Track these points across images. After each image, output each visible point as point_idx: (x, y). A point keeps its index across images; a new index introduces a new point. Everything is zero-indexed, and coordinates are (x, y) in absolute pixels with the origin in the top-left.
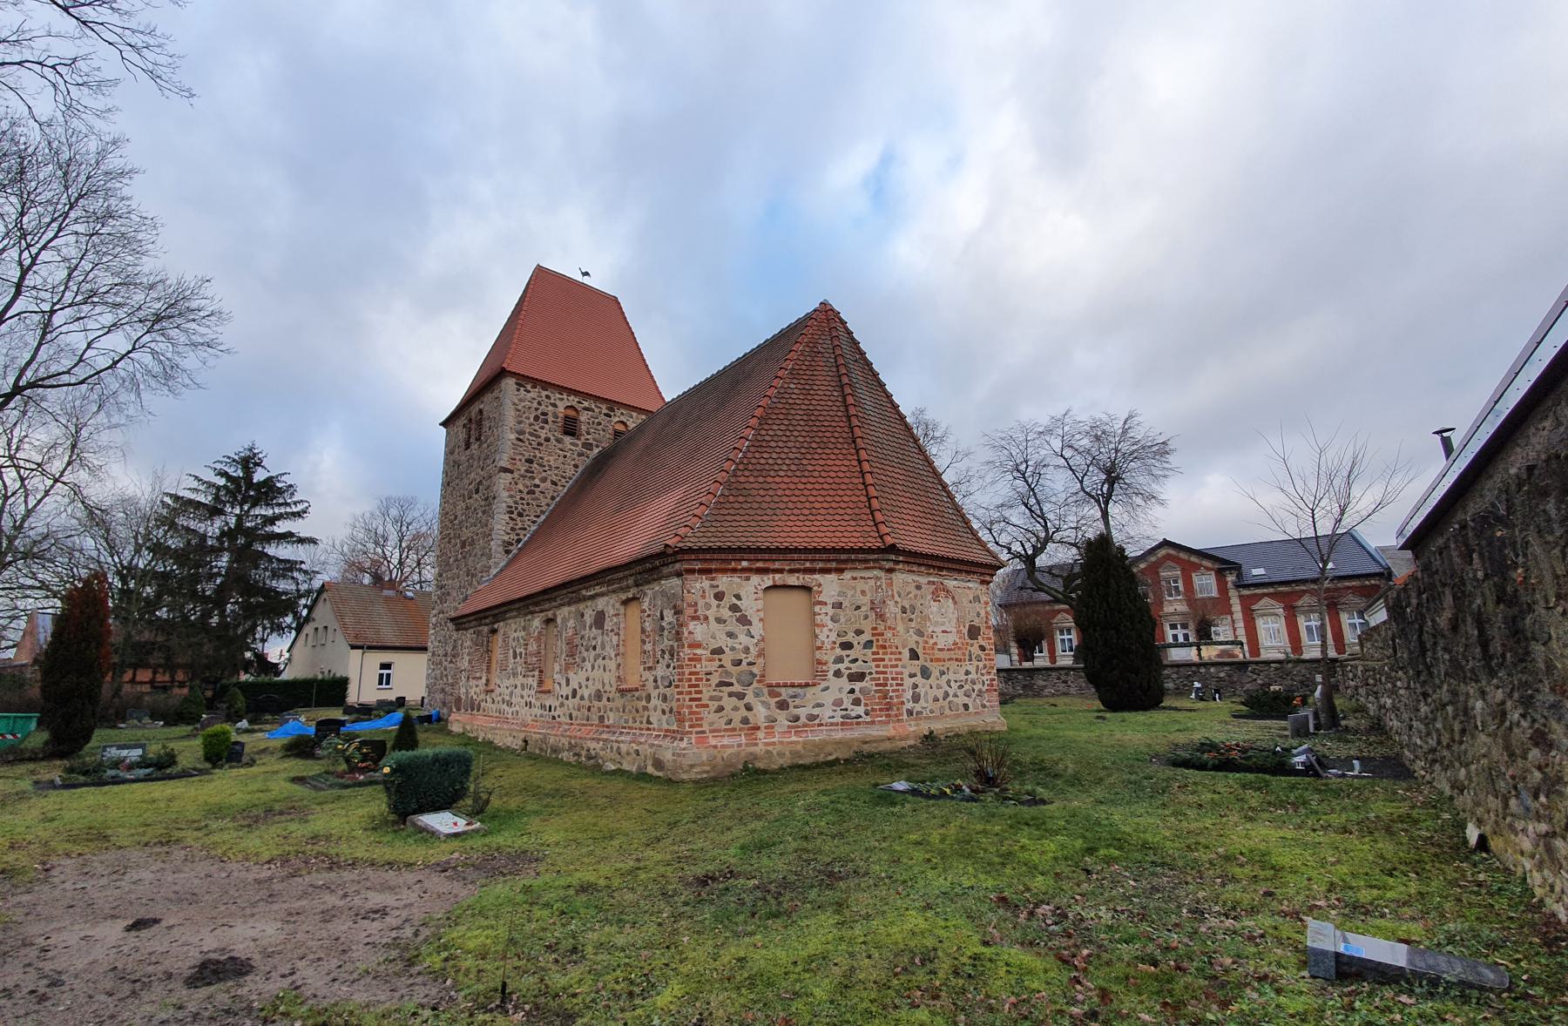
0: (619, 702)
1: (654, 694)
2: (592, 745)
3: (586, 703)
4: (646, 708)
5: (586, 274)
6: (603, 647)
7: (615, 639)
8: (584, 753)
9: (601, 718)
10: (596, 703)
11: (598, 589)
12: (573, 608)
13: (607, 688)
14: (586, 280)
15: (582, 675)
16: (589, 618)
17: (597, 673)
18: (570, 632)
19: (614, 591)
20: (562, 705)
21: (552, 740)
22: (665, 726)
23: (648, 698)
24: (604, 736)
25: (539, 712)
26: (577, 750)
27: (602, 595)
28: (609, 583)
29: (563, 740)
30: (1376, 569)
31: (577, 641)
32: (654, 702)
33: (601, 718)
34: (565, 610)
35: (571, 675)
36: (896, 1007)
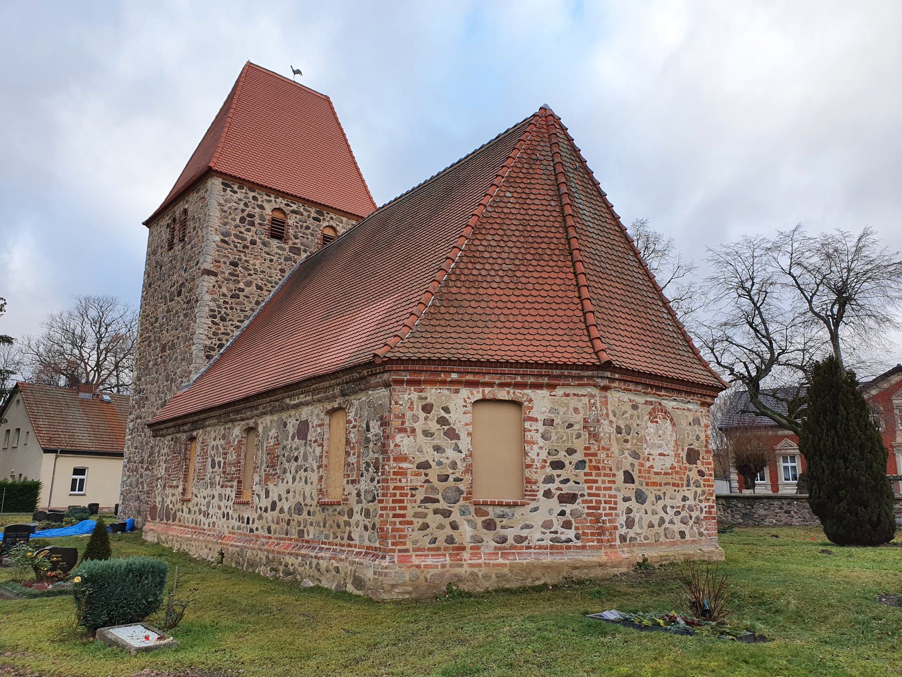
0: (319, 517)
1: (357, 508)
2: (290, 560)
4: (347, 524)
6: (305, 459)
7: (318, 450)
8: (281, 568)
9: (301, 533)
10: (295, 517)
13: (308, 501)
15: (282, 488)
18: (272, 442)
20: (260, 518)
23: (351, 513)
24: (303, 551)
25: (237, 524)
27: (307, 404)
28: (315, 392)
29: (261, 554)
31: (278, 451)
32: (356, 517)
33: (301, 533)
34: (268, 419)
35: (271, 486)
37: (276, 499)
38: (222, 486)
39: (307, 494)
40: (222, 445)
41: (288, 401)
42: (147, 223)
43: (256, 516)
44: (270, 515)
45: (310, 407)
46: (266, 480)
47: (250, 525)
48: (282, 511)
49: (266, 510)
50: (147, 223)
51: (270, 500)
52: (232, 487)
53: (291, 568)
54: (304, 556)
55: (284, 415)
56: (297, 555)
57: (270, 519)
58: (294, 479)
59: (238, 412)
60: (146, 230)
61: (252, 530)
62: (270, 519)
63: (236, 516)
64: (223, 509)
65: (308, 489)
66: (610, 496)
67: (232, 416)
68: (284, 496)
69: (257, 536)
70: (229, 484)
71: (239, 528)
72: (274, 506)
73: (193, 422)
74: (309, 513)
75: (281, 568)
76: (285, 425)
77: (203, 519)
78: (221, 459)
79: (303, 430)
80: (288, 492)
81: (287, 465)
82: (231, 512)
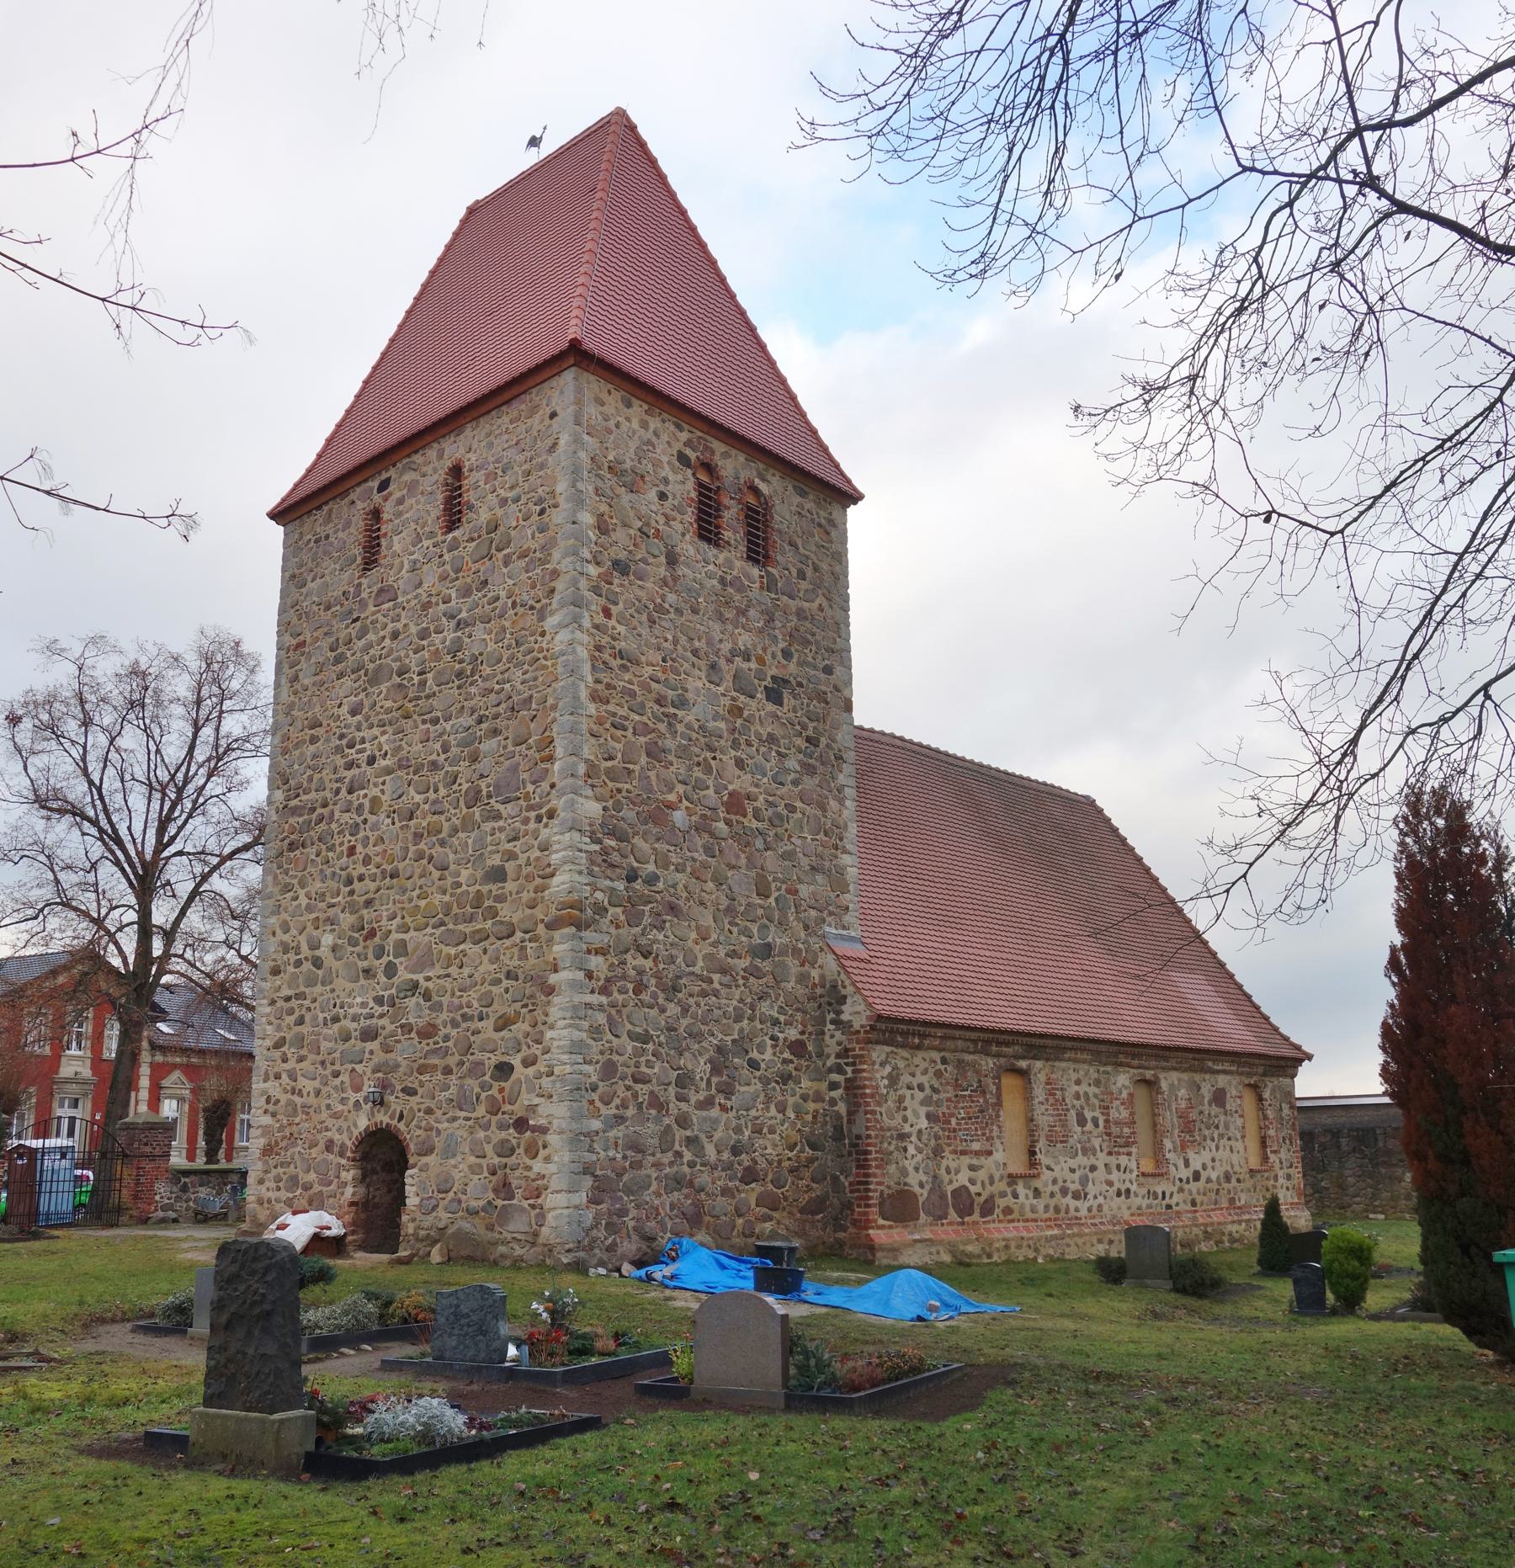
0: (1249, 1183)
1: (1281, 1173)
2: (1234, 1228)
3: (1215, 1186)
4: (1274, 1187)
5: (534, 142)
6: (1227, 1127)
7: (1239, 1122)
8: (1225, 1239)
9: (1232, 1201)
10: (1226, 1186)
11: (1226, 1066)
12: (1185, 1076)
13: (1237, 1169)
14: (548, 148)
15: (1206, 1156)
16: (1206, 1091)
17: (1223, 1154)
18: (1183, 1105)
19: (1241, 1074)
20: (1181, 1190)
21: (1180, 1233)
22: (1290, 1200)
23: (1276, 1178)
24: (1246, 1217)
25: (1145, 1202)
26: (1217, 1237)
27: (1225, 1072)
28: (1239, 1064)
29: (1196, 1230)
30: (1239, 1037)
31: (1193, 1115)
32: (1281, 1181)
33: (1232, 1201)
34: (1174, 1076)
35: (1191, 1155)
36: (702, 903)
37: (1199, 1168)
38: (1110, 1153)
39: (1235, 1162)
40: (1096, 1096)
41: (1210, 1064)
42: (277, 515)
43: (1175, 1189)
44: (1193, 1186)
45: (1229, 1077)
46: (1183, 1148)
47: (1167, 1200)
48: (1209, 1180)
49: (1188, 1182)
50: (277, 515)
51: (1191, 1169)
52: (1129, 1154)
53: (1237, 1236)
54: (1248, 1221)
55: (1197, 1077)
56: (1240, 1222)
57: (1194, 1191)
58: (1217, 1148)
59: (1134, 1056)
60: (278, 531)
61: (1169, 1207)
62: (1194, 1191)
63: (1144, 1191)
64: (1117, 1185)
65: (1235, 1158)
66: (858, 1191)
67: (1122, 1058)
68: (1209, 1164)
69: (1178, 1213)
70: (1125, 1150)
71: (1149, 1207)
72: (1196, 1176)
73: (1031, 1046)
74: (1239, 1181)
75: (1225, 1239)
76: (1199, 1088)
77: (1073, 1203)
78: (1097, 1114)
79: (1219, 1098)
80: (1213, 1160)
81: (1207, 1132)
82: (1134, 1188)
